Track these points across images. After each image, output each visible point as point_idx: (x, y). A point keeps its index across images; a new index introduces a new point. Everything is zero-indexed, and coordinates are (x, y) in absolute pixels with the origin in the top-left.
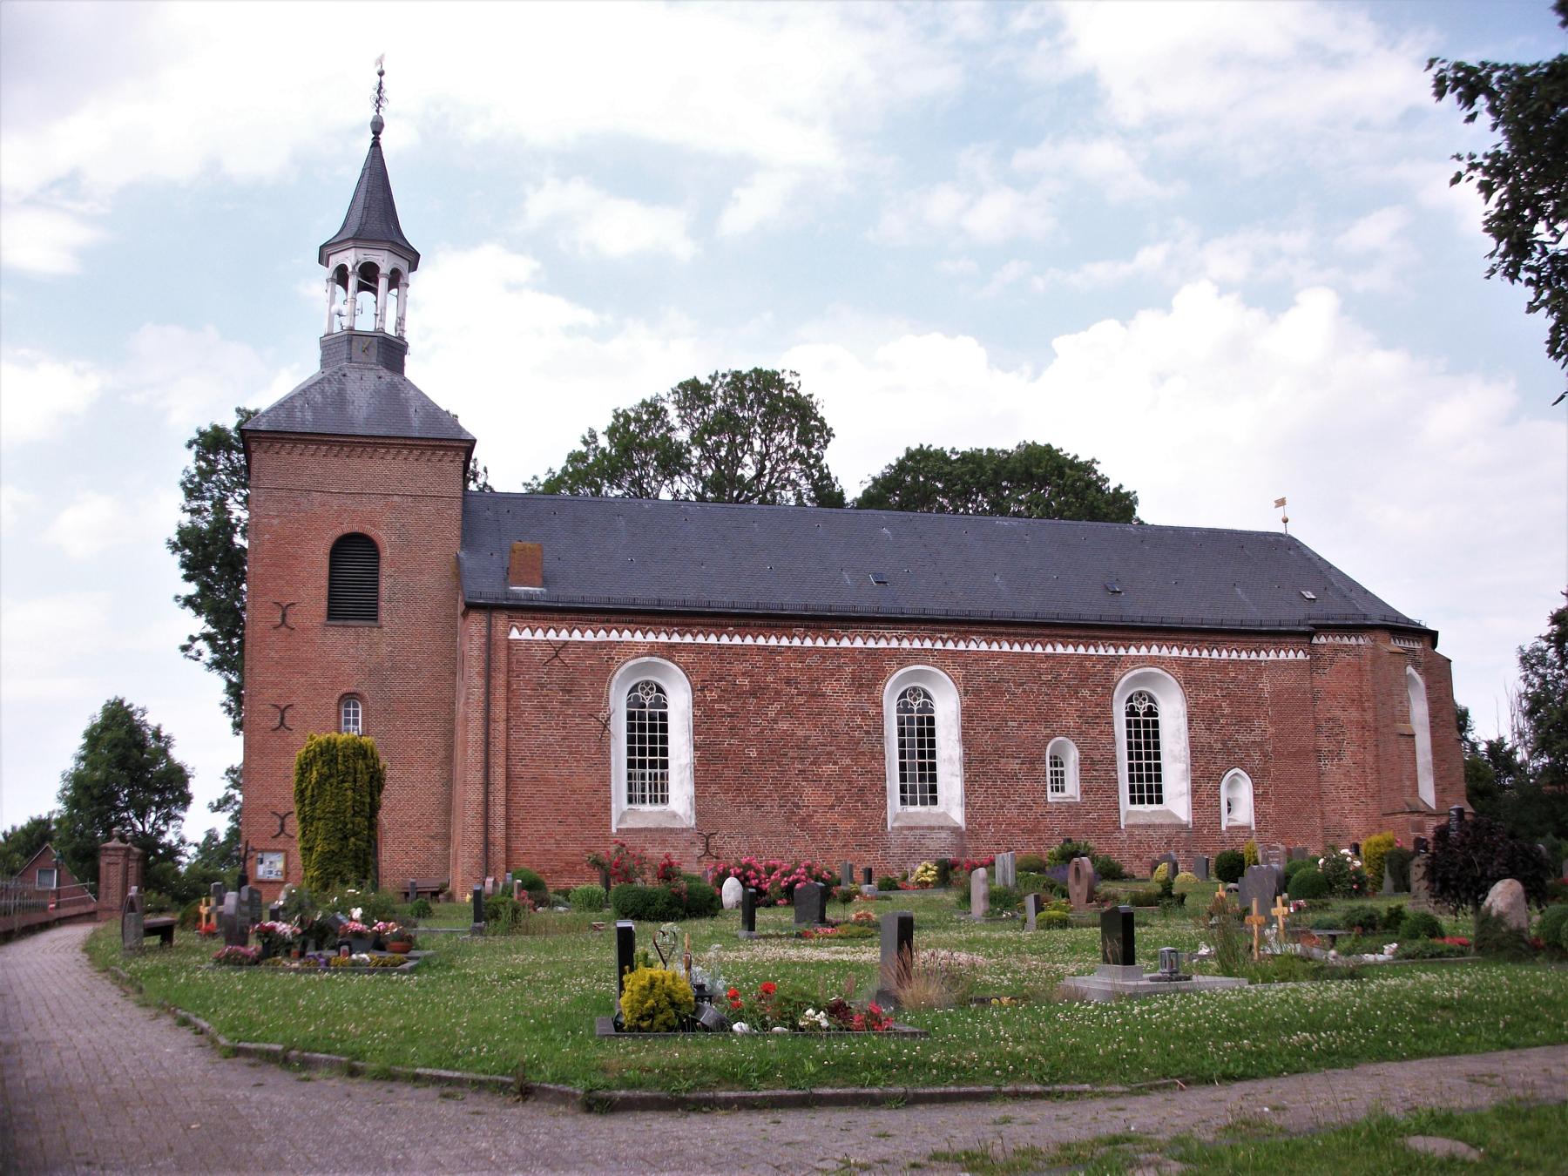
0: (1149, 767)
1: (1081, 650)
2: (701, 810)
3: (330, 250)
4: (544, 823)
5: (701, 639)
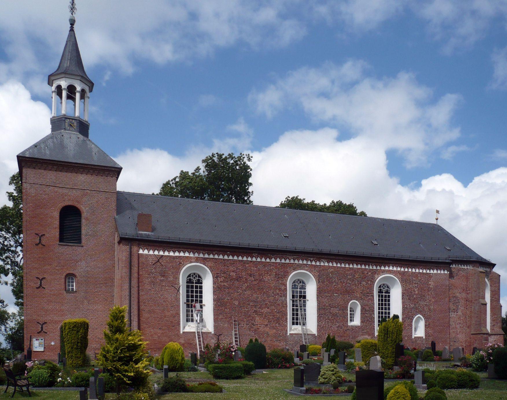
0: (386, 313)
1: (363, 267)
2: (216, 327)
3: (52, 78)
4: (153, 329)
5: (216, 257)
